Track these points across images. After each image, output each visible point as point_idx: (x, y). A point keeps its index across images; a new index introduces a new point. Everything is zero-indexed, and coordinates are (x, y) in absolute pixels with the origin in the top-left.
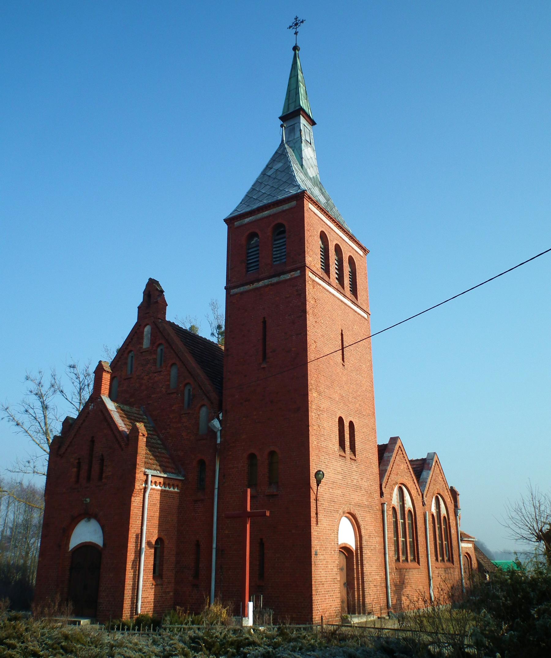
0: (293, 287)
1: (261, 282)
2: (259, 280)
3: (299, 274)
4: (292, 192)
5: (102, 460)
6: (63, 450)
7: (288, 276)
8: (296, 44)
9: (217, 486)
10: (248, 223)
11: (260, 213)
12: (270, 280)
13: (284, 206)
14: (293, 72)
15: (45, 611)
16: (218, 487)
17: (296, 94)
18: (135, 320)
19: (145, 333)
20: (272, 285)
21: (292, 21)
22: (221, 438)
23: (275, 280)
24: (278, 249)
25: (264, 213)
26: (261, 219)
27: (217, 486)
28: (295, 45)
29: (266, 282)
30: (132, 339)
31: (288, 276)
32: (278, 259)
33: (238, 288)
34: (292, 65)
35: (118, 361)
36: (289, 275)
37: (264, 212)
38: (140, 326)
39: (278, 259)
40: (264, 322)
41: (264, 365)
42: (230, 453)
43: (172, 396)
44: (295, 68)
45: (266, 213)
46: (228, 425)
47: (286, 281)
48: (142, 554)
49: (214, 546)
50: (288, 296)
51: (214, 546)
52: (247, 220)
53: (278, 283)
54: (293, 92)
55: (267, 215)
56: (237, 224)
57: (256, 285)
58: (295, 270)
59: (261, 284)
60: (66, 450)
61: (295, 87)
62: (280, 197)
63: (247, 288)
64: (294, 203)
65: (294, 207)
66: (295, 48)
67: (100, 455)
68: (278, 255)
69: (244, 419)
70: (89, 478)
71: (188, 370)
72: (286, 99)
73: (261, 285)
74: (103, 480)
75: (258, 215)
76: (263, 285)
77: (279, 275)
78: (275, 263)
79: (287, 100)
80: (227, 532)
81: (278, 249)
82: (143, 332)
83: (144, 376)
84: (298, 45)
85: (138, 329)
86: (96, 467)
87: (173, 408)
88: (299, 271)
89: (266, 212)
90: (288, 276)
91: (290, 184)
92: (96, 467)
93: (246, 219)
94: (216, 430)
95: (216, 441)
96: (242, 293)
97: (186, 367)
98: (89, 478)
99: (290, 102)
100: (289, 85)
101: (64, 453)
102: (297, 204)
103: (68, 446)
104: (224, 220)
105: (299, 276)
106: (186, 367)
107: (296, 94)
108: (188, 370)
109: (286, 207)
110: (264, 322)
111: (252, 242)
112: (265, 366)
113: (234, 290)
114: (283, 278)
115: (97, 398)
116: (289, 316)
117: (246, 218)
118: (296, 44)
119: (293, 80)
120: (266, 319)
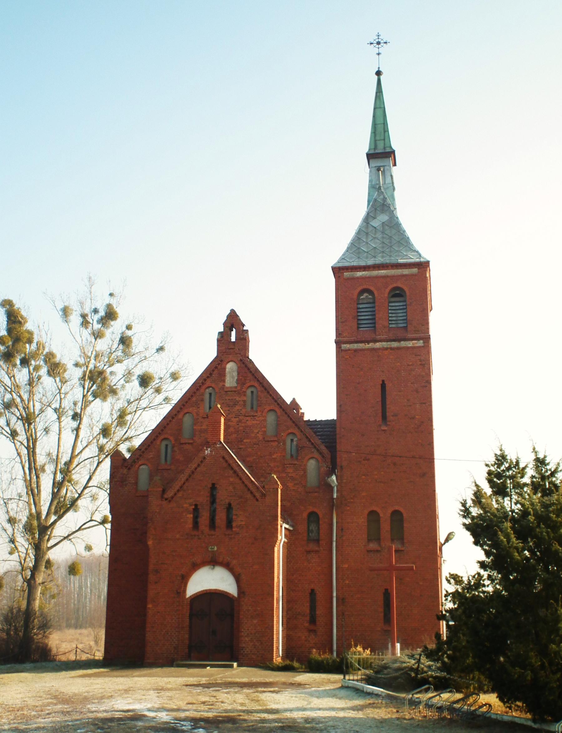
0: (416, 356)
1: (378, 343)
2: (375, 341)
3: (423, 345)
4: (412, 257)
5: (229, 508)
6: (169, 494)
7: (410, 344)
8: (379, 68)
9: (335, 539)
10: (362, 278)
11: (376, 270)
12: (389, 343)
13: (404, 270)
14: (378, 101)
15: (359, 649)
16: (336, 539)
17: (385, 132)
18: (213, 354)
19: (227, 370)
20: (391, 349)
21: (373, 38)
22: (337, 493)
23: (395, 344)
24: (393, 312)
25: (380, 271)
26: (377, 277)
27: (335, 539)
28: (377, 70)
29: (385, 344)
30: (211, 374)
31: (410, 344)
32: (393, 322)
33: (350, 344)
34: (376, 93)
35: (192, 396)
36: (411, 343)
37: (380, 270)
38: (222, 361)
39: (393, 322)
40: (383, 386)
41: (384, 428)
42: (348, 508)
43: (272, 444)
44: (380, 99)
45: (383, 272)
46: (345, 481)
47: (408, 348)
48: (104, 600)
49: (335, 594)
50: (411, 363)
51: (335, 594)
52: (359, 274)
53: (398, 348)
54: (380, 128)
55: (383, 274)
56: (347, 274)
57: (371, 345)
58: (418, 339)
59: (378, 345)
60: (175, 494)
61: (382, 122)
62: (401, 261)
63: (361, 346)
64: (415, 270)
65: (416, 275)
66: (379, 73)
67: (227, 503)
68: (394, 319)
69: (363, 477)
70: (212, 525)
71: (291, 419)
72: (371, 133)
73: (378, 347)
74: (234, 529)
75: (374, 272)
76: (381, 346)
77: (399, 340)
78: (391, 326)
79: (373, 134)
80: (347, 582)
81: (393, 312)
82: (225, 369)
83: (232, 418)
84: (380, 69)
85: (219, 364)
86: (221, 517)
87: (273, 457)
88: (422, 341)
89: (382, 271)
90: (410, 344)
91: (406, 246)
92: (221, 517)
93: (358, 273)
94: (333, 485)
95: (332, 495)
96: (356, 351)
97: (289, 416)
98: (212, 525)
99: (378, 138)
100: (374, 116)
101: (172, 497)
102: (419, 272)
103: (178, 491)
104: (332, 267)
105: (423, 347)
106: (289, 416)
107: (385, 132)
108: (291, 419)
109: (406, 272)
110: (383, 386)
111: (362, 297)
112: (386, 428)
113: (345, 345)
114: (403, 344)
115: (215, 443)
116: (412, 383)
117: (358, 271)
118: (379, 68)
119: (379, 112)
120: (385, 382)
